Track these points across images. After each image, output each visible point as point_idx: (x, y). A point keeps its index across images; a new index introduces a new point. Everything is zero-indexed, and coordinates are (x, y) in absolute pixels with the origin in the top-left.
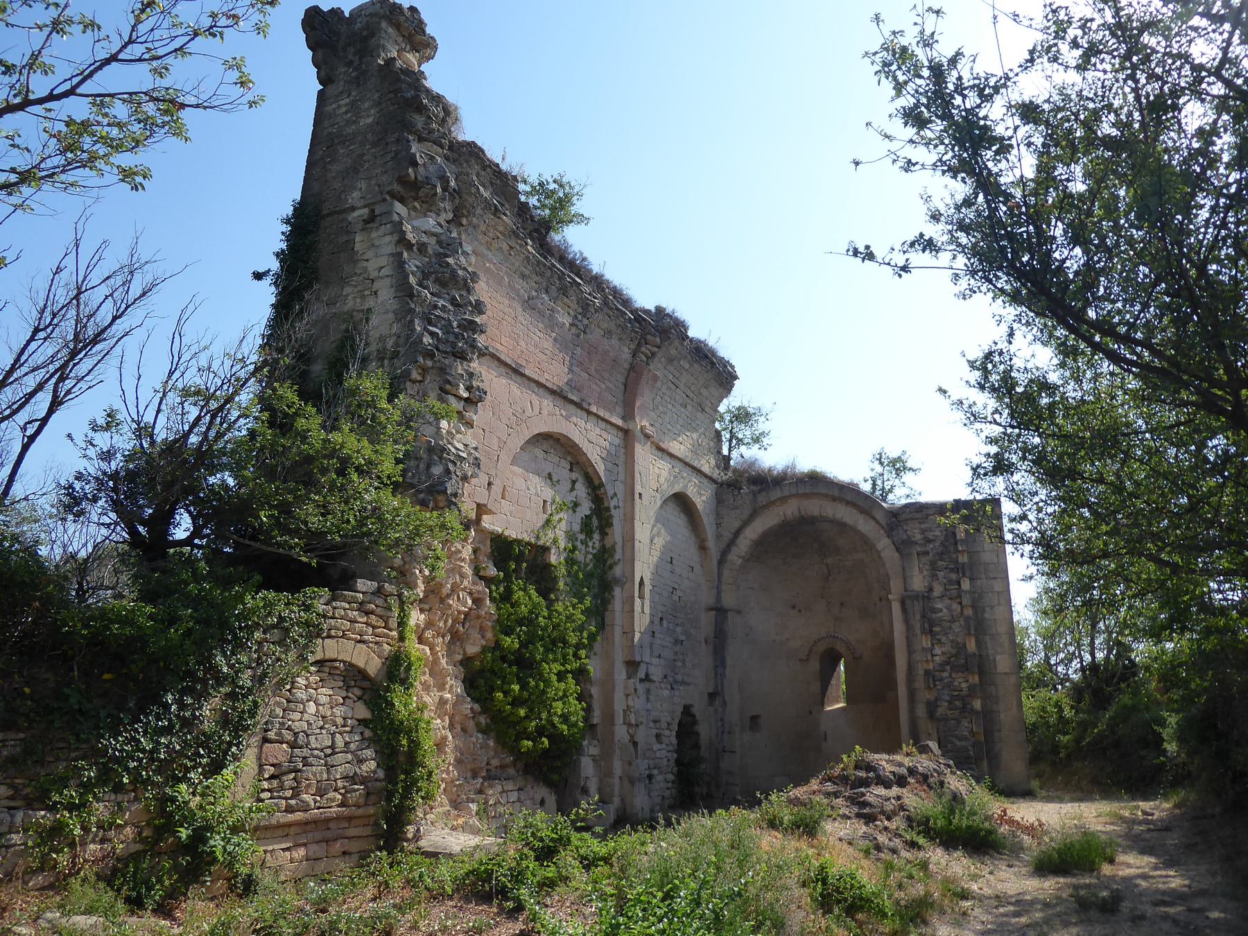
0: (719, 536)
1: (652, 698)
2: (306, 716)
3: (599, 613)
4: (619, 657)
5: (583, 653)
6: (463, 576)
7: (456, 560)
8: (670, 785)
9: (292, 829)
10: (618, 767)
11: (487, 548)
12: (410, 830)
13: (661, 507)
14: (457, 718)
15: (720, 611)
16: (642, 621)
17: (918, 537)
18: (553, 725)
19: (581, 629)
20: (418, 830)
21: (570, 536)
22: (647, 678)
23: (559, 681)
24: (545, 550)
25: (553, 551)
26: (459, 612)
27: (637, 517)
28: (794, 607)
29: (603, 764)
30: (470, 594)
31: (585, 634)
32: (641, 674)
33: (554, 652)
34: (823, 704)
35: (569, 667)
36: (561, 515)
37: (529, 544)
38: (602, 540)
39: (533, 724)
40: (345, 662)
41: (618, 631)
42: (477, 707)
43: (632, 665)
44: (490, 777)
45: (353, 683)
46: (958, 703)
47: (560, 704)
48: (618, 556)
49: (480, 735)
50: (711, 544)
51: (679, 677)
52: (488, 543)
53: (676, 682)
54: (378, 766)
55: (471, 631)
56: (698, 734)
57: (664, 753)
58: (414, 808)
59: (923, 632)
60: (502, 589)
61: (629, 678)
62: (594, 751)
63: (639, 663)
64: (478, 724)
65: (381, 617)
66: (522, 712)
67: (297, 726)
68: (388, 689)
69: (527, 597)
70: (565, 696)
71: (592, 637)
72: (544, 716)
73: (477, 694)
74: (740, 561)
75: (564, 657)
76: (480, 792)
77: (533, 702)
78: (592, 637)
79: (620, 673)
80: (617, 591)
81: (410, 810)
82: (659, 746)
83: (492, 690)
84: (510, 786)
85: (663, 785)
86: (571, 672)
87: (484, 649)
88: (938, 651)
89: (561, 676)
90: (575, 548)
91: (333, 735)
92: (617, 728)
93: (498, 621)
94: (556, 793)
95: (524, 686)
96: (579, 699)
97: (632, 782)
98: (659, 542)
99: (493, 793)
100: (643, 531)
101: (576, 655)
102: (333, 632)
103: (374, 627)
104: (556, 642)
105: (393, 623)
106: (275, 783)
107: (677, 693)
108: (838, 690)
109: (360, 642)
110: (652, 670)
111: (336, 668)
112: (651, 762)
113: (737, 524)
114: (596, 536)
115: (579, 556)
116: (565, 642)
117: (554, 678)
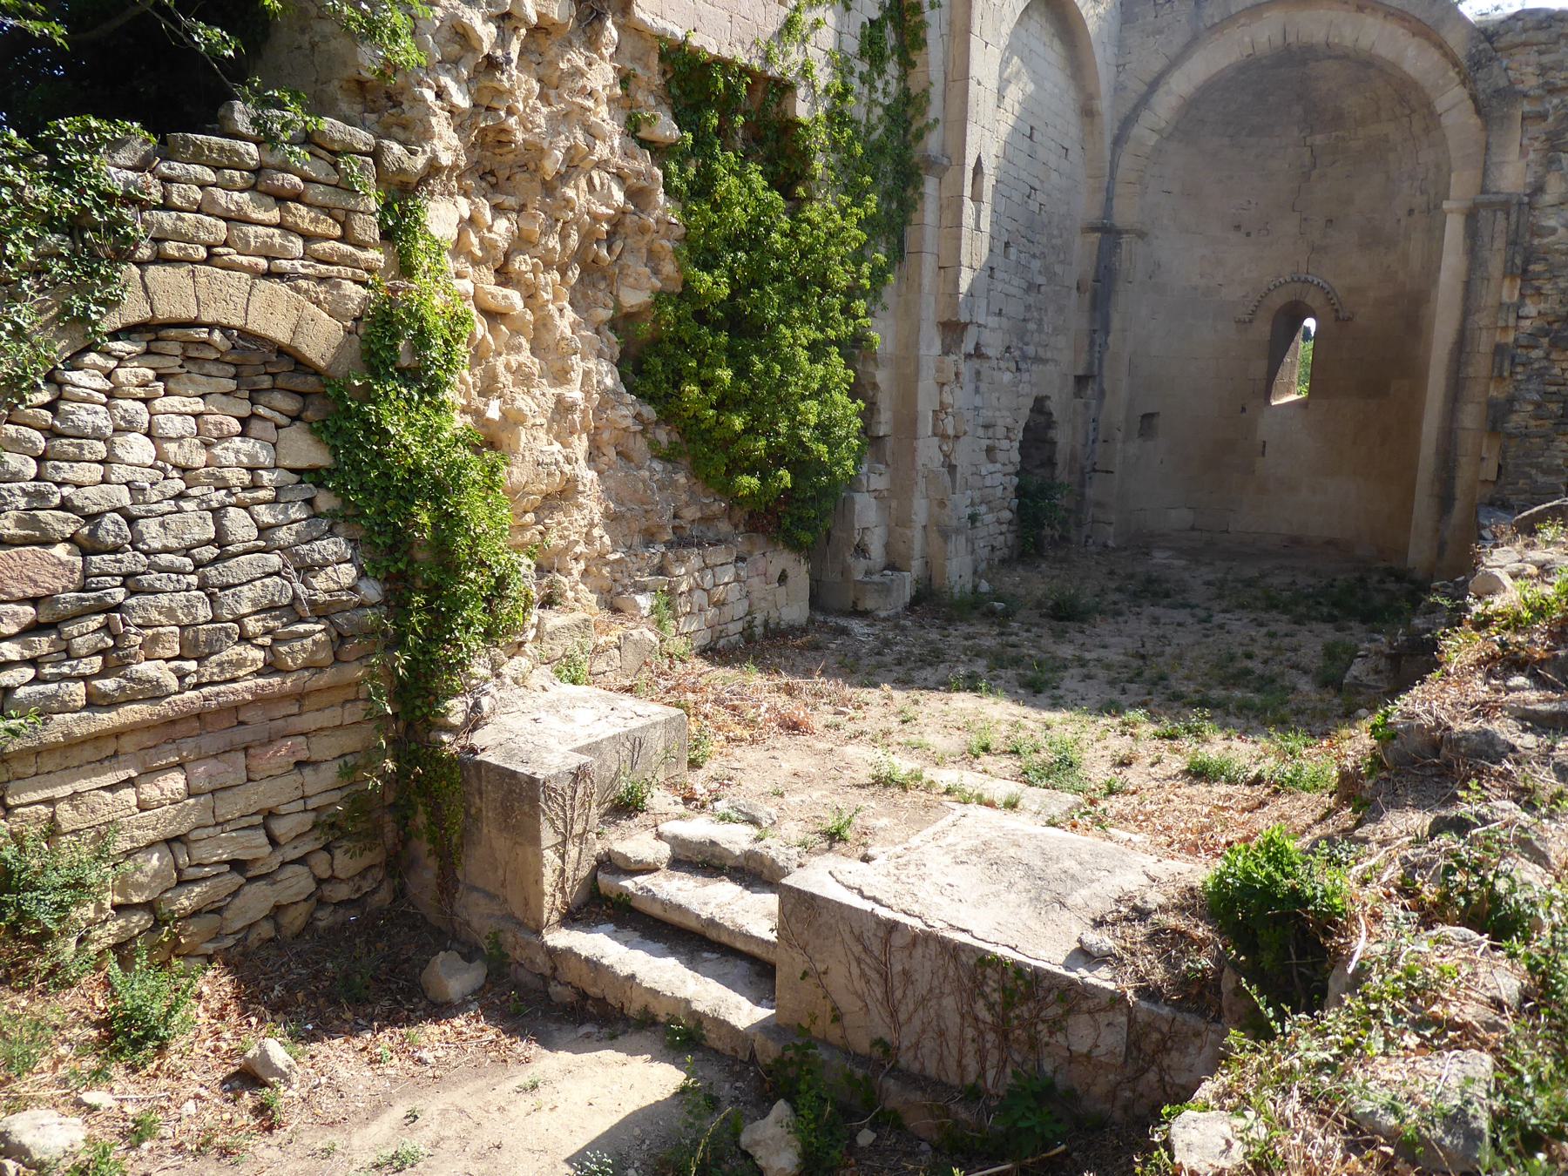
0: (1119, 89)
1: (984, 386)
2: (120, 472)
3: (893, 227)
4: (930, 313)
5: (860, 306)
6: (591, 133)
7: (572, 92)
8: (1004, 528)
9: (124, 740)
10: (920, 510)
11: (651, 74)
12: (456, 710)
13: (1020, 22)
14: (606, 436)
15: (1108, 233)
16: (975, 248)
17: (1531, 82)
18: (801, 444)
19: (858, 257)
20: (477, 705)
21: (842, 66)
22: (978, 353)
23: (812, 361)
24: (783, 88)
25: (801, 92)
26: (596, 218)
27: (976, 29)
28: (1238, 227)
29: (894, 504)
30: (620, 177)
31: (866, 269)
32: (968, 346)
33: (806, 305)
34: (1268, 394)
35: (832, 333)
36: (819, 13)
37: (746, 70)
38: (903, 78)
39: (762, 443)
40: (225, 329)
41: (929, 263)
42: (649, 412)
43: (953, 330)
44: (681, 542)
45: (266, 382)
46: (1554, 407)
47: (813, 405)
48: (934, 111)
49: (658, 466)
50: (1104, 104)
51: (1030, 350)
52: (654, 60)
53: (1025, 357)
54: (362, 574)
55: (628, 259)
56: (1053, 443)
57: (999, 478)
58: (461, 662)
59: (1509, 273)
60: (692, 171)
61: (946, 352)
62: (879, 482)
63: (966, 325)
64: (653, 444)
65: (328, 210)
66: (738, 423)
67: (91, 498)
68: (367, 395)
69: (744, 188)
70: (824, 388)
71: (879, 275)
72: (783, 427)
73: (649, 388)
74: (1153, 139)
75: (824, 313)
76: (661, 570)
77: (761, 403)
78: (879, 275)
79: (931, 345)
80: (930, 186)
81: (451, 669)
82: (991, 467)
83: (677, 379)
84: (717, 555)
85: (993, 529)
86: (838, 342)
87: (660, 298)
88: (1531, 309)
89: (817, 351)
90: (847, 91)
91: (218, 513)
92: (920, 444)
93: (685, 238)
94: (808, 558)
95: (742, 372)
96: (853, 394)
97: (945, 535)
98: (1014, 94)
99: (684, 575)
100: (985, 63)
101: (846, 310)
102: (171, 248)
103: (308, 238)
104: (807, 284)
105: (367, 228)
106: (43, 644)
107: (1026, 377)
108: (1292, 373)
109: (269, 275)
110: (987, 337)
111: (206, 343)
112: (977, 495)
113: (1157, 65)
114: (892, 68)
115: (855, 107)
116: (825, 285)
117: (802, 355)
